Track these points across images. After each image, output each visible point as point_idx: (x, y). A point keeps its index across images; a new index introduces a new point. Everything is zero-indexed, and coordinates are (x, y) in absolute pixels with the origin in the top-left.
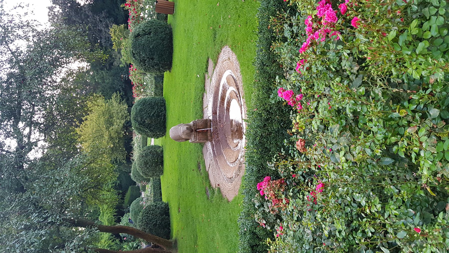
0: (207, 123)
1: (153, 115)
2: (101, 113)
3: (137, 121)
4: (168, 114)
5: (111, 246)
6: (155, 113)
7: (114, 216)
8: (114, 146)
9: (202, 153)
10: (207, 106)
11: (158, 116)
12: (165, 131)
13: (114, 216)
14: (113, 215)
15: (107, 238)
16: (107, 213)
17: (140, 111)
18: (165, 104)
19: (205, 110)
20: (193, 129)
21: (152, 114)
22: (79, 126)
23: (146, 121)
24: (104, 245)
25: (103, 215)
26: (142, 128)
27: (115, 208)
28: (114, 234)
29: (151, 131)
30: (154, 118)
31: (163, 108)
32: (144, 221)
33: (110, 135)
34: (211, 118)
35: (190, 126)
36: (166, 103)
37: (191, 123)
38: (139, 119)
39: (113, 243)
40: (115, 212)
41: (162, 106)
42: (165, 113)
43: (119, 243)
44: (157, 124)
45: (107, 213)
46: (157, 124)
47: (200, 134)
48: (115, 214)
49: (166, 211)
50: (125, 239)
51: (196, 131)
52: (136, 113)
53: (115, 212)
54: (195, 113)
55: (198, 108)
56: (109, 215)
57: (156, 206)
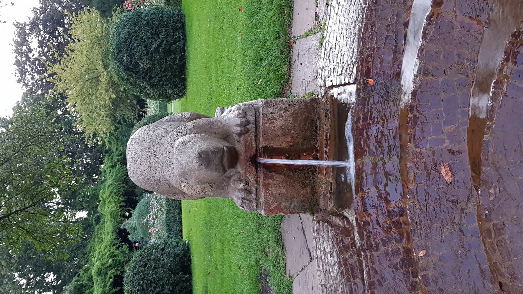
0: (317, 124)
1: (157, 49)
2: (95, 40)
3: (121, 62)
4: (190, 49)
5: (114, 256)
6: (160, 45)
7: (120, 207)
8: (118, 97)
9: (280, 243)
10: (319, 27)
11: (168, 52)
12: (185, 88)
13: (120, 207)
14: (118, 205)
15: (109, 243)
16: (110, 202)
17: (126, 40)
18: (183, 24)
19: (303, 47)
20: (240, 147)
21: (154, 47)
22: (60, 61)
23: (140, 62)
24: (104, 252)
25: (104, 204)
26: (132, 80)
27: (122, 195)
28: (120, 237)
29: (153, 86)
30: (158, 57)
31: (178, 34)
32: (136, 283)
33: (111, 78)
34: (348, 94)
35: (226, 136)
36: (187, 21)
37: (230, 115)
38: (125, 59)
39: (117, 252)
40: (123, 201)
41: (177, 29)
42: (184, 45)
43: (127, 252)
44: (166, 70)
45: (110, 202)
46: (166, 70)
47: (278, 178)
48: (123, 204)
49: (183, 263)
50: (137, 244)
51: (254, 161)
52: (119, 44)
53: (123, 201)
54: (251, 54)
55: (266, 34)
56: (113, 205)
57: (163, 249)
